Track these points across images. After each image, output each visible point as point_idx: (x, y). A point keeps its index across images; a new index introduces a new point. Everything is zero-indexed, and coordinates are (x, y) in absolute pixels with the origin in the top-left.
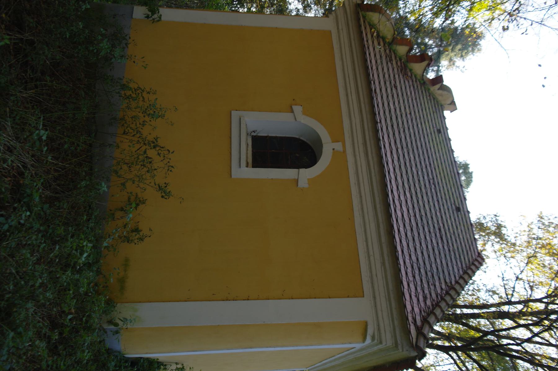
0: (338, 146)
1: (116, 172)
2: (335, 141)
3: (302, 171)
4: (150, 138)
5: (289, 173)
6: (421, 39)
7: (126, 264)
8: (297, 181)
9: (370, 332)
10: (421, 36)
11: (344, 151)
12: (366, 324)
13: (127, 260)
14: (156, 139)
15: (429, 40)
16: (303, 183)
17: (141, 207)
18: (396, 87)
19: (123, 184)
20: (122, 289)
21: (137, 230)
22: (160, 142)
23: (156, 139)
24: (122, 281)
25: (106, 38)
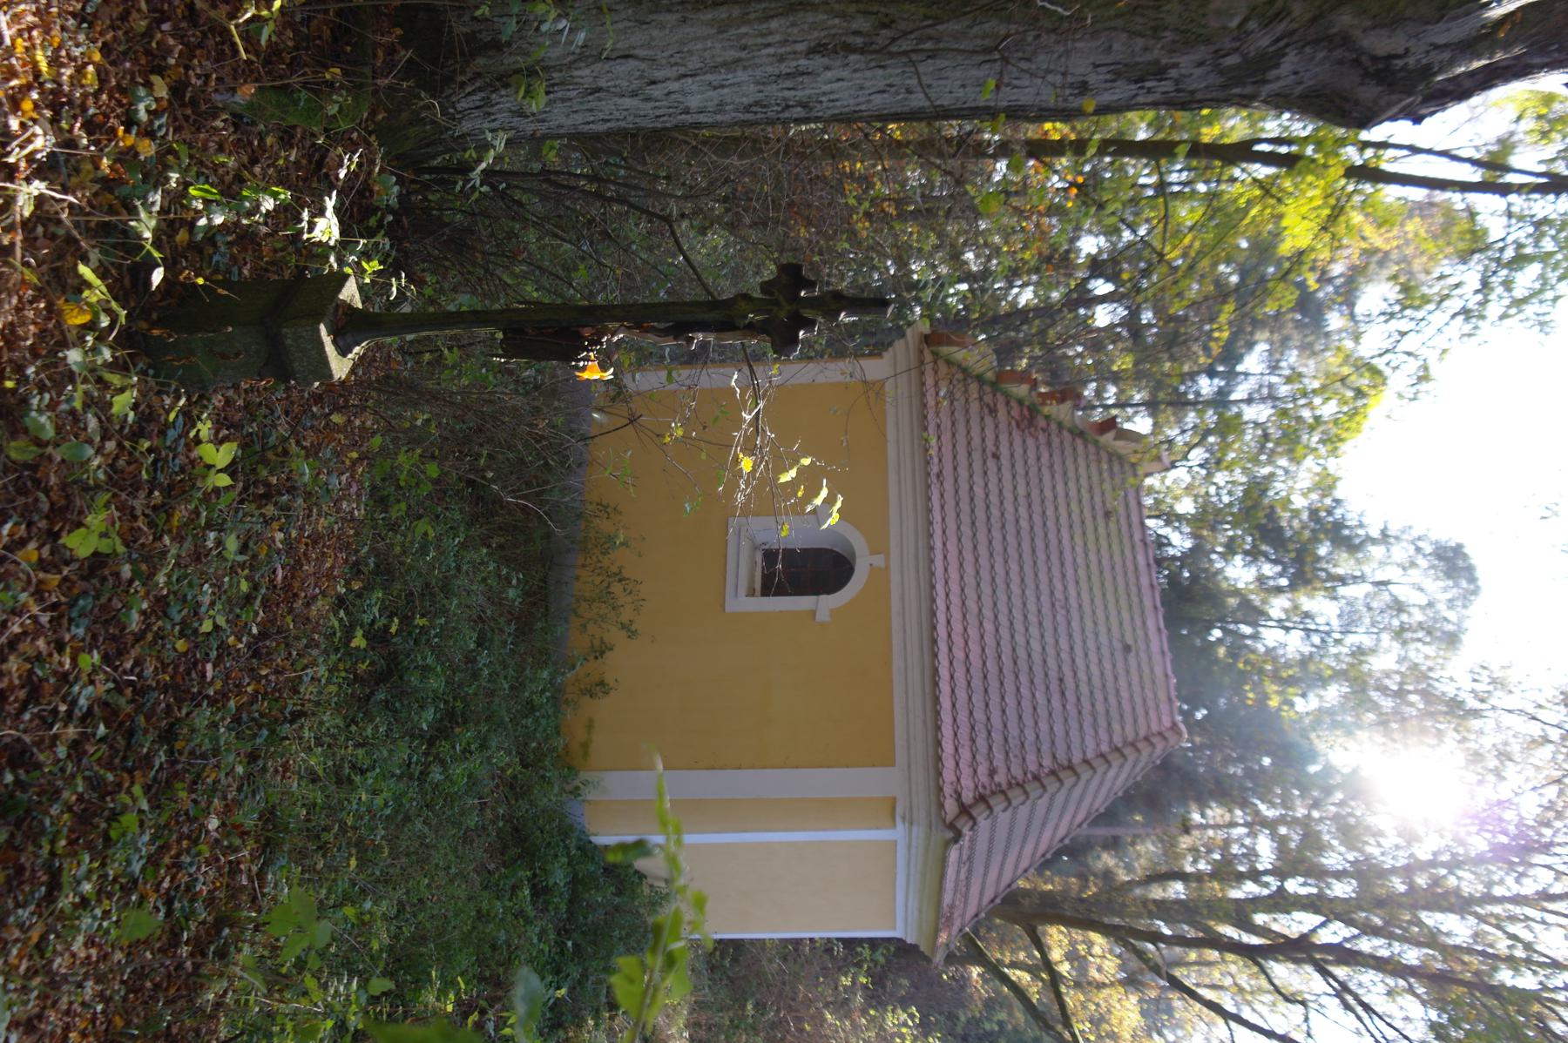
0: (879, 561)
1: (575, 611)
2: (874, 552)
3: (823, 598)
4: (614, 569)
5: (803, 603)
6: (198, 995)
7: (590, 725)
8: (813, 613)
9: (899, 810)
10: (987, 230)
11: (887, 567)
12: (894, 800)
13: (591, 721)
14: (621, 568)
15: (913, 272)
16: (823, 616)
17: (608, 654)
18: (996, 456)
19: (584, 626)
20: (586, 754)
21: (602, 683)
22: (625, 574)
23: (621, 568)
24: (585, 746)
25: (1224, 302)
